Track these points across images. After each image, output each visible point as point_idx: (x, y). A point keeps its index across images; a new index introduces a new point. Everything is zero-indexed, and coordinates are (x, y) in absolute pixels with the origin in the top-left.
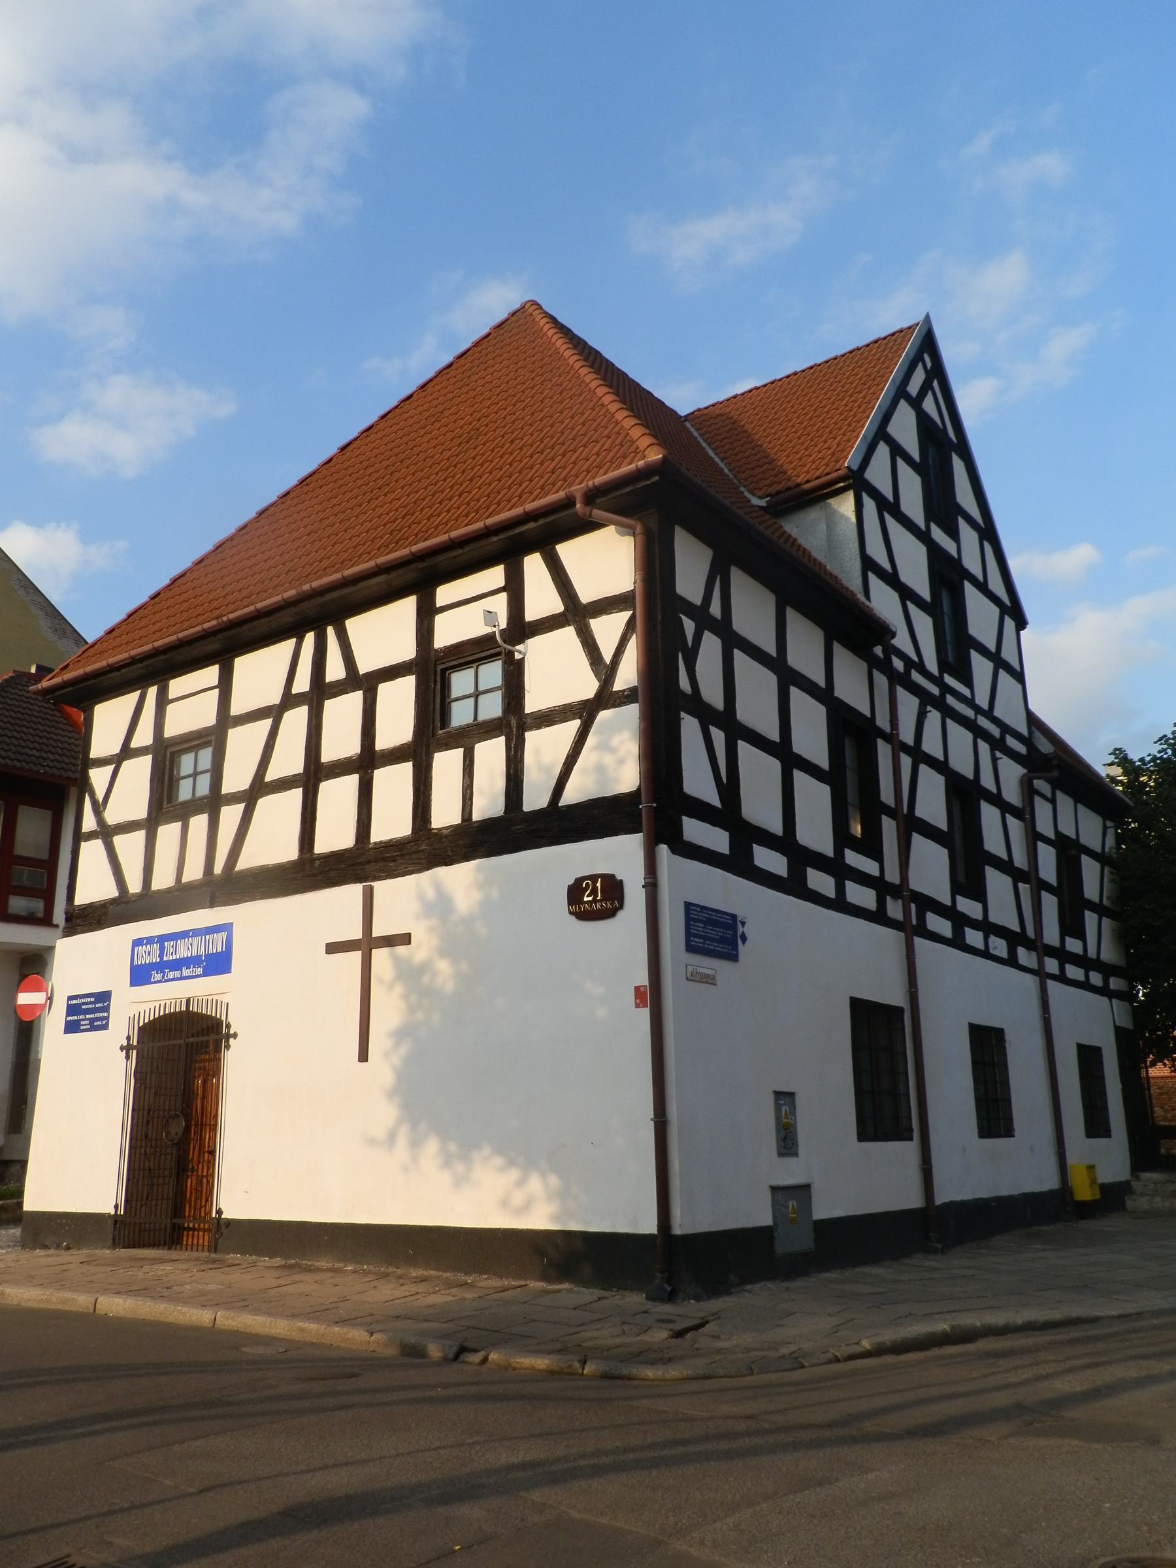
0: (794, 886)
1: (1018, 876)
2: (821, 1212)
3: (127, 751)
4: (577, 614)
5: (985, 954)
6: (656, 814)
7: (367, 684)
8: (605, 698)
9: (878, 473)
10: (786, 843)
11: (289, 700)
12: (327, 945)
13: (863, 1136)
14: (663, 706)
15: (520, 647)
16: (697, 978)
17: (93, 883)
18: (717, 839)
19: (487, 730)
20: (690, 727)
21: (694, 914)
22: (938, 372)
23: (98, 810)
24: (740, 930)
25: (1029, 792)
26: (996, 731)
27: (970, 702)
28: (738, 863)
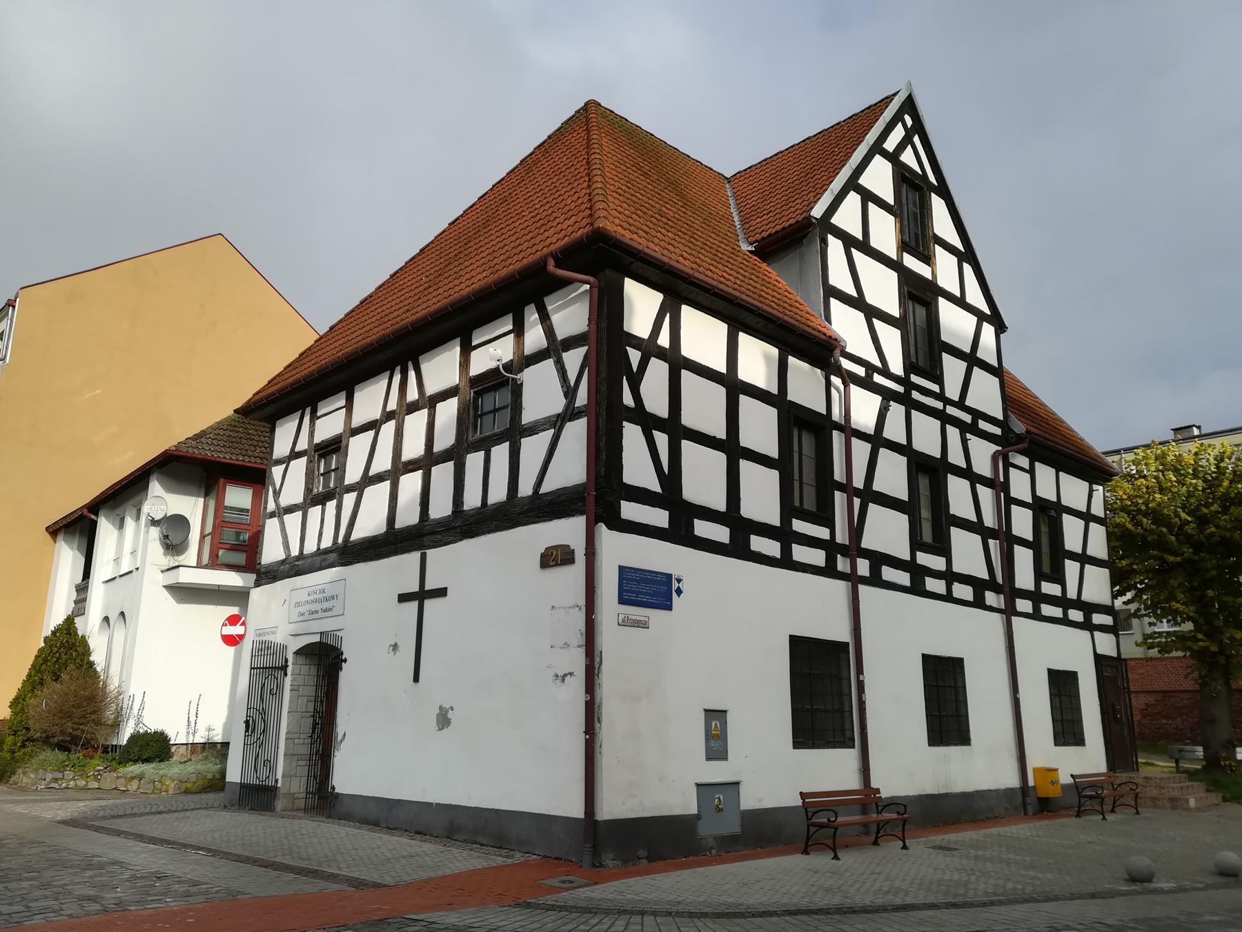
0: (738, 549)
1: (986, 534)
2: (749, 800)
3: (295, 455)
4: (555, 349)
5: (948, 598)
8: (571, 413)
9: (848, 217)
10: (731, 516)
11: (388, 416)
13: (797, 745)
14: (607, 415)
17: (272, 552)
18: (659, 517)
19: (497, 439)
20: (632, 434)
22: (918, 128)
23: (277, 494)
24: (675, 585)
25: (1002, 460)
26: (967, 418)
27: (941, 396)
28: (680, 531)
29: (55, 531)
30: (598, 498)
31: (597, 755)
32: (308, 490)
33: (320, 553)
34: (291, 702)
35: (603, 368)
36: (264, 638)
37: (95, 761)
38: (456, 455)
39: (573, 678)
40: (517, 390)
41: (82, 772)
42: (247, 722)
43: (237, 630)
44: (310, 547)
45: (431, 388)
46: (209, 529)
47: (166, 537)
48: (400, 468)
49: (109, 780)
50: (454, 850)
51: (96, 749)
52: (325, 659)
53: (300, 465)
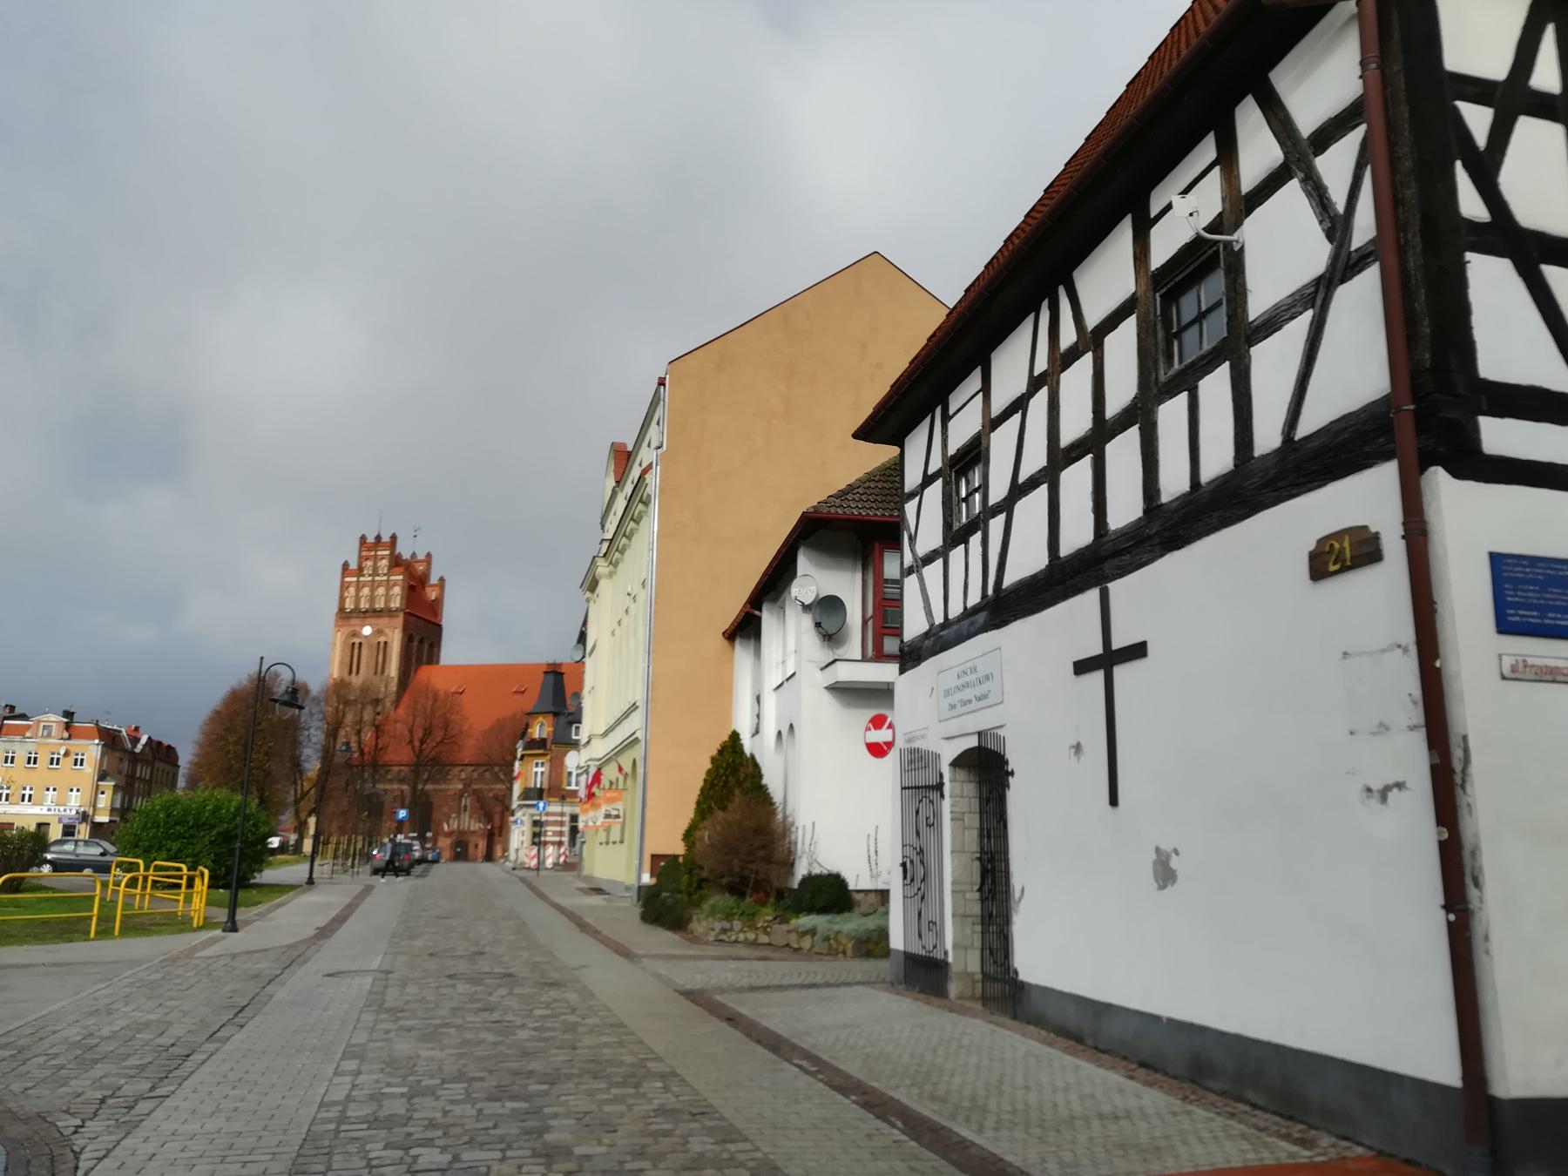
3: (928, 480)
6: (1422, 419)
7: (1092, 341)
8: (1344, 267)
12: (1076, 664)
15: (1235, 237)
16: (1519, 674)
19: (1206, 365)
20: (1491, 282)
21: (1508, 573)
23: (912, 539)
29: (731, 636)
30: (1420, 417)
31: (1480, 958)
32: (947, 525)
33: (968, 613)
34: (954, 838)
35: (1404, 150)
36: (916, 745)
37: (764, 910)
38: (1141, 414)
39: (1404, 794)
40: (1235, 263)
41: (750, 919)
42: (904, 865)
43: (882, 736)
44: (956, 609)
45: (1094, 316)
46: (870, 612)
47: (818, 625)
48: (1060, 457)
49: (780, 933)
50: (1201, 1113)
51: (768, 895)
52: (987, 767)
53: (935, 492)
